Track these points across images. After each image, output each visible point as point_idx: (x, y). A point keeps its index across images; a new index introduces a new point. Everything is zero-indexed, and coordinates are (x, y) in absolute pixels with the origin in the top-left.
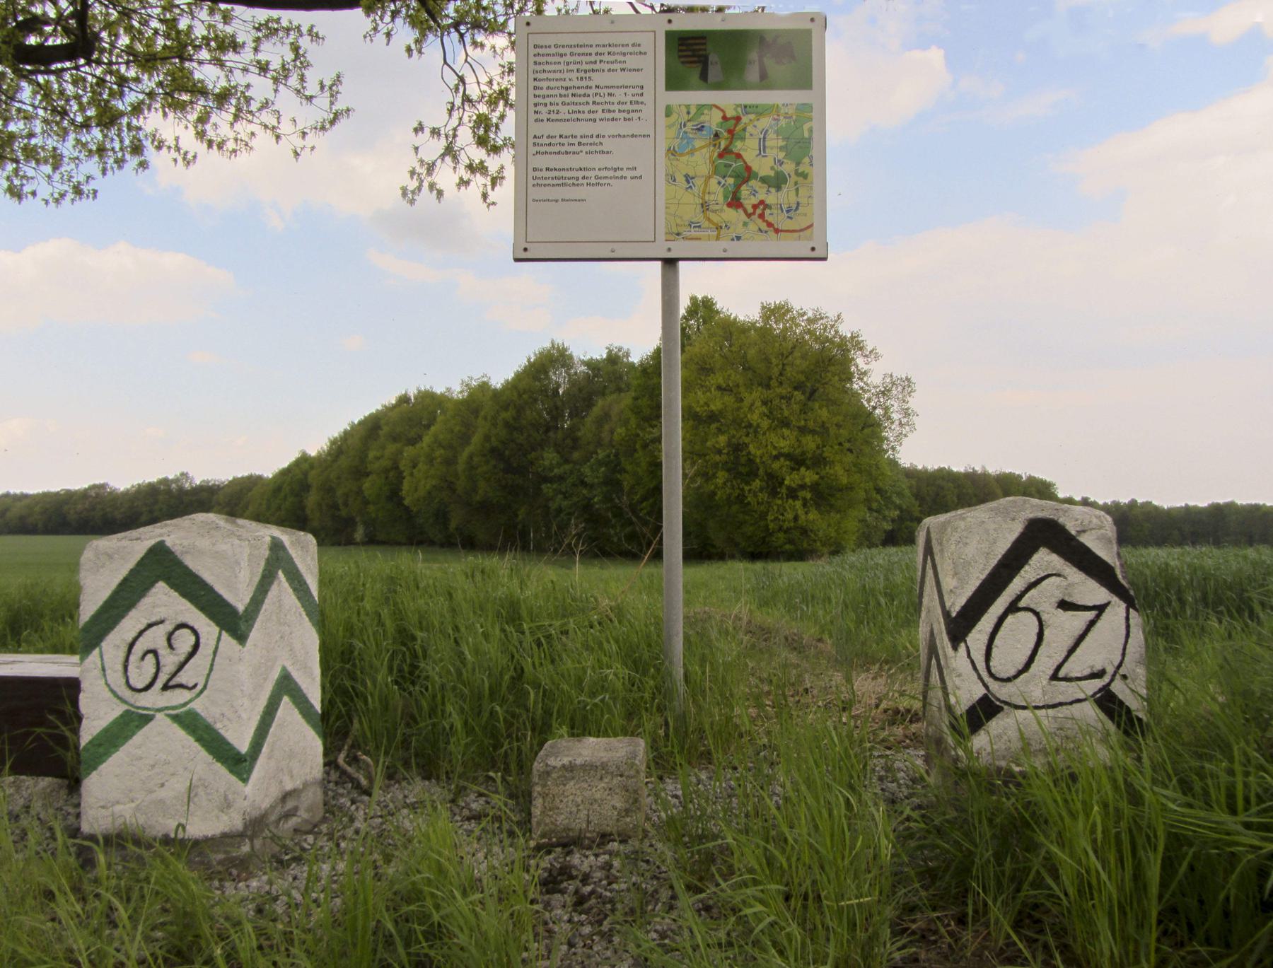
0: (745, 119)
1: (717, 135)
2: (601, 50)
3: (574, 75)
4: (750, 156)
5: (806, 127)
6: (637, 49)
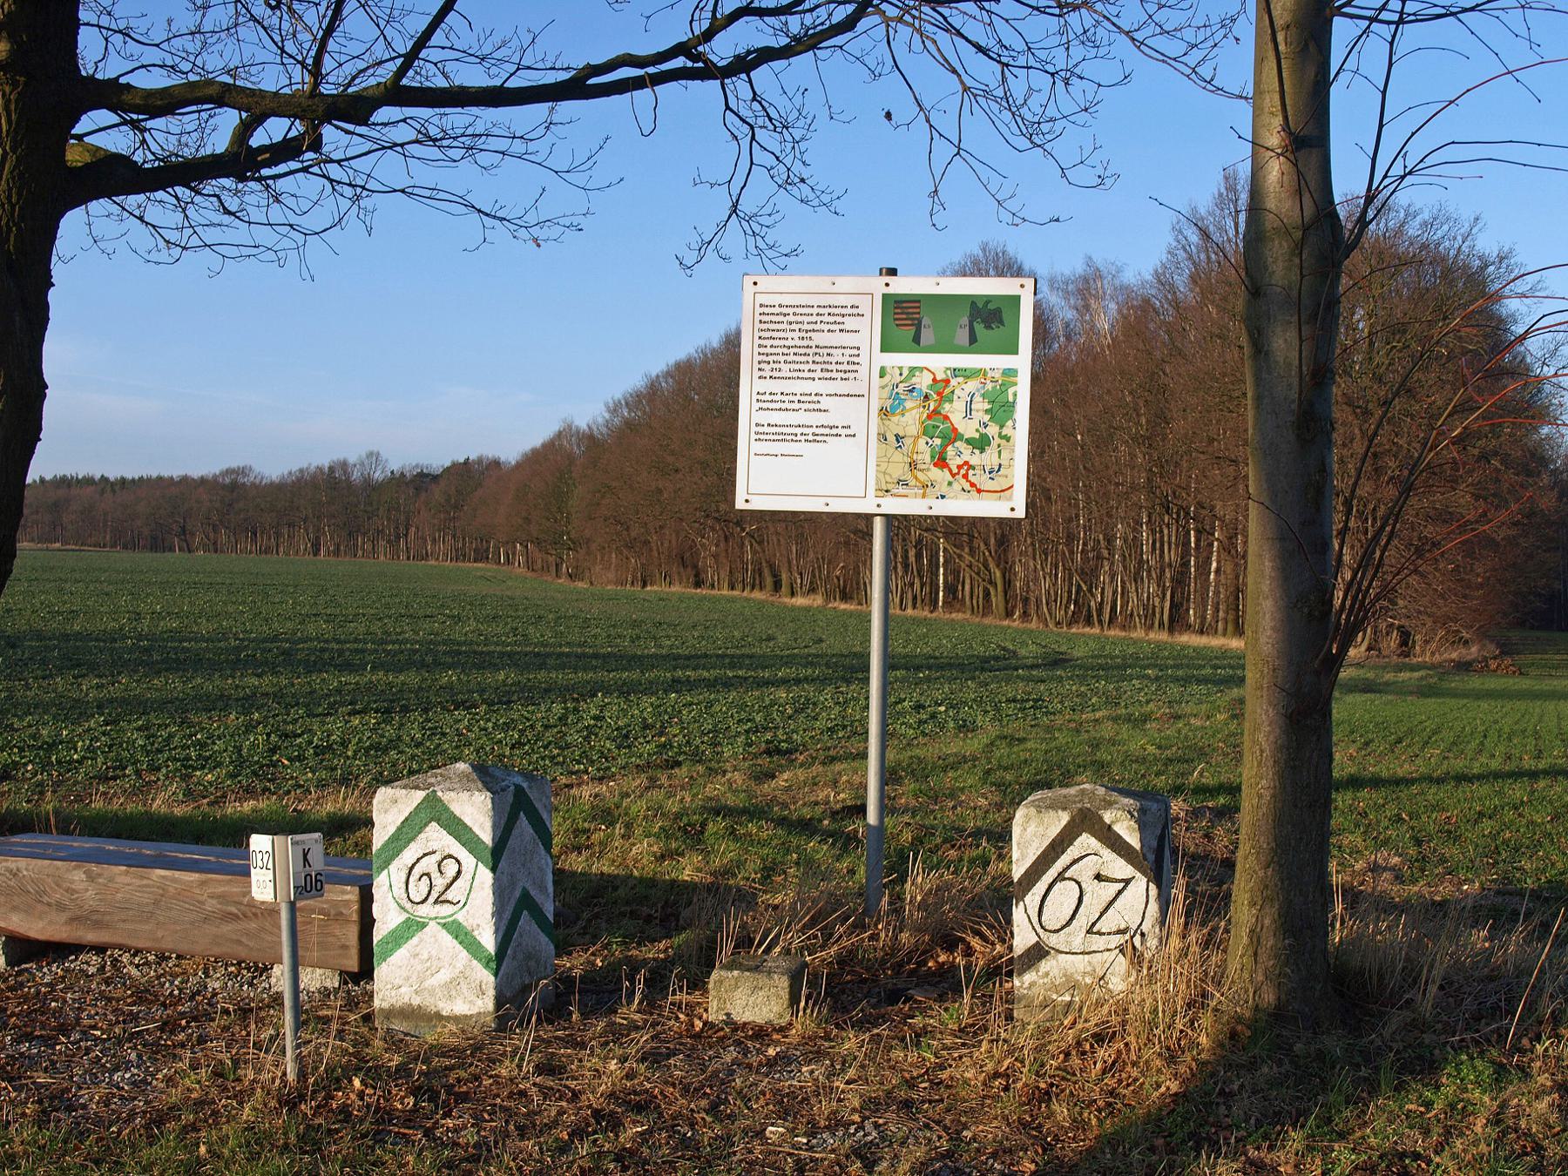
0: (953, 382)
1: (926, 397)
2: (821, 311)
3: (796, 335)
4: (957, 418)
5: (1011, 391)
6: (855, 311)
